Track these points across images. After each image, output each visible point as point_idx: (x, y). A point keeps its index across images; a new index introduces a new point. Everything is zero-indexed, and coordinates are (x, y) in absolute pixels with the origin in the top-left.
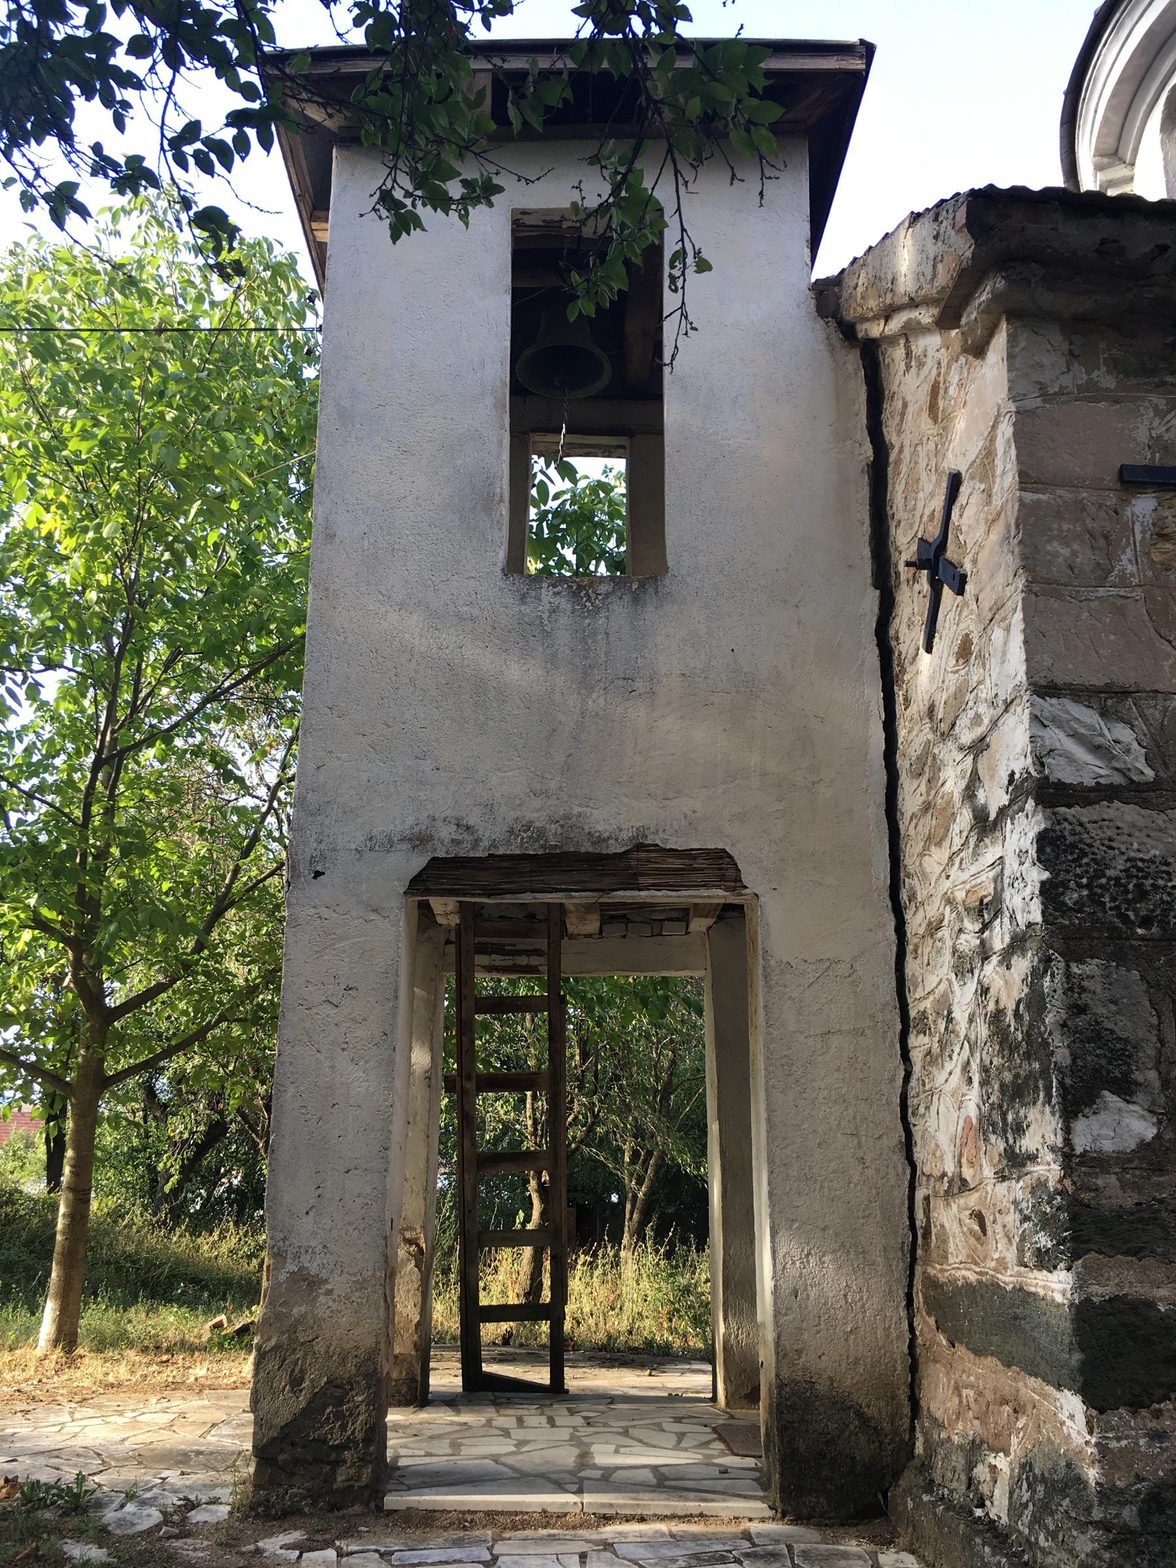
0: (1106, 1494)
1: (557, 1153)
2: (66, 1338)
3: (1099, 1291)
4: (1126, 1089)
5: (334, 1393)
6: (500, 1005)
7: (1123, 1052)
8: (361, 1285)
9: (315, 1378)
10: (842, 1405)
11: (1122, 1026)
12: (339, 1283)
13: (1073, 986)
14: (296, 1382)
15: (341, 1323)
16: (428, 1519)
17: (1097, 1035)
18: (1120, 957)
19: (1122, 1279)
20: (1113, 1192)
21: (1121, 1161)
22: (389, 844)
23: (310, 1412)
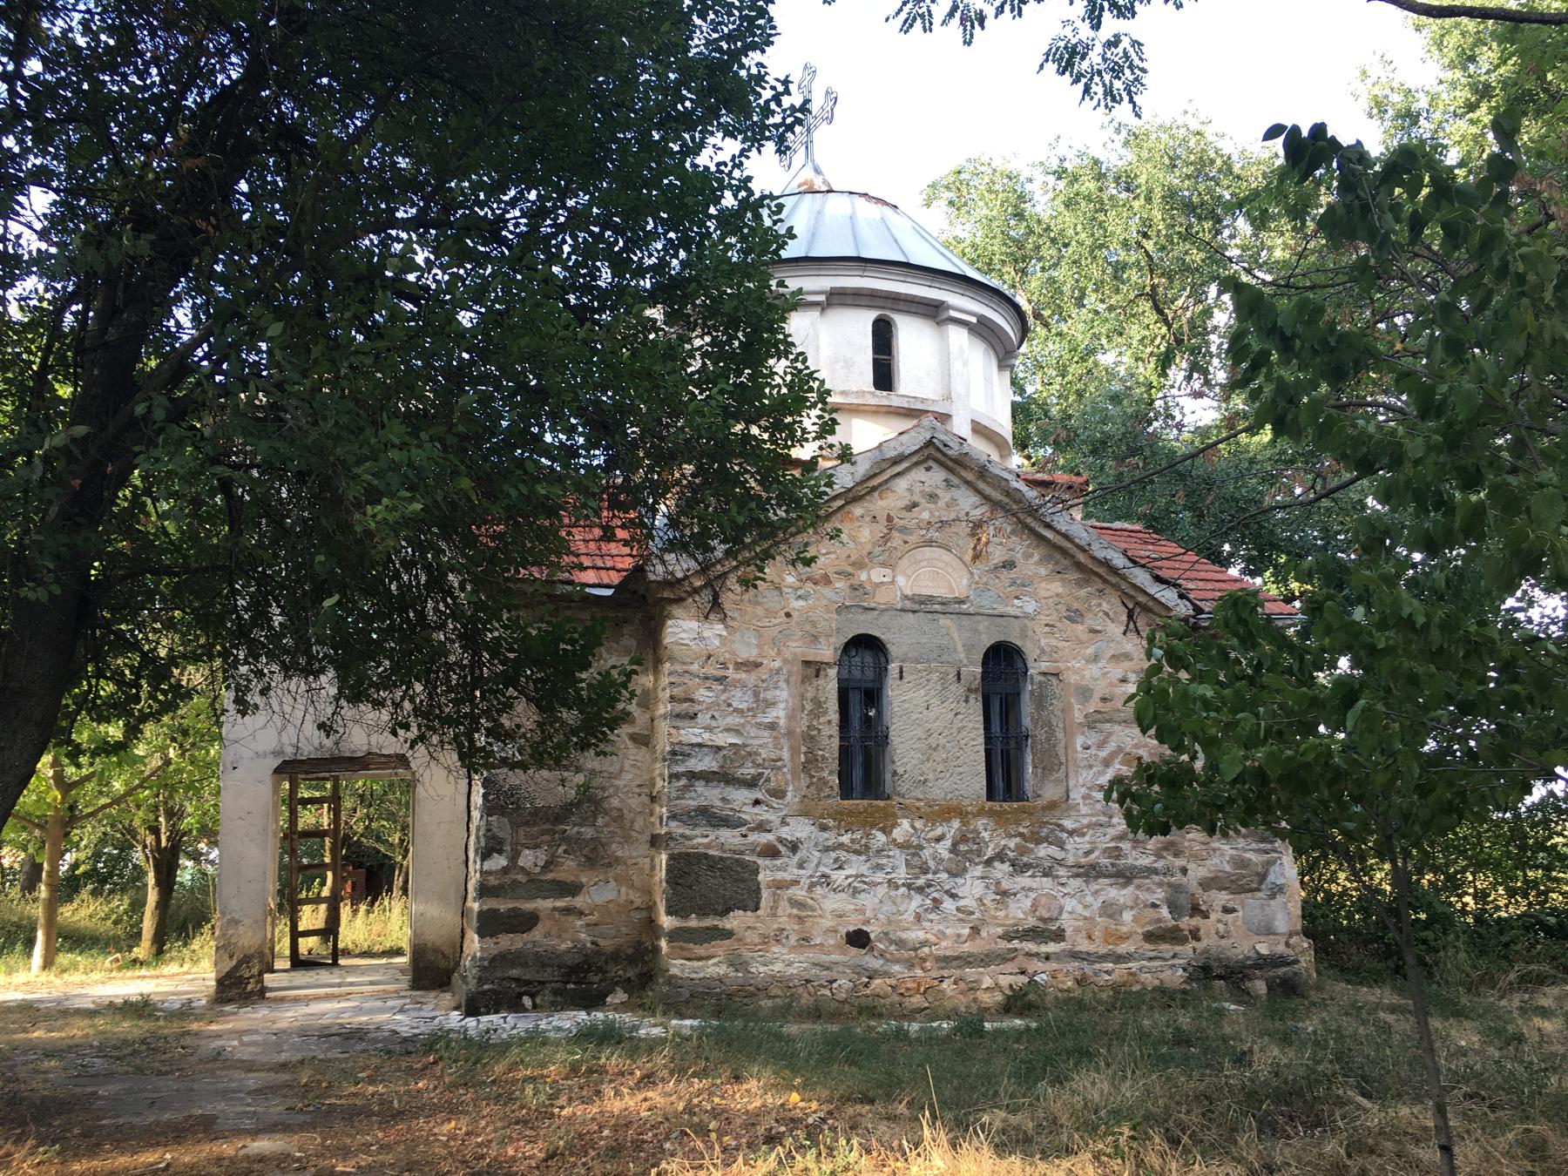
0: (482, 959)
1: (342, 840)
2: (48, 964)
3: (485, 908)
4: (500, 852)
5: (246, 960)
6: (305, 802)
7: (501, 842)
8: (256, 922)
9: (238, 956)
10: (436, 950)
11: (501, 834)
12: (247, 922)
13: (488, 823)
14: (231, 957)
15: (247, 939)
16: (282, 1000)
17: (494, 837)
18: (503, 815)
19: (492, 904)
20: (493, 881)
21: (497, 872)
22: (265, 755)
23: (237, 967)
